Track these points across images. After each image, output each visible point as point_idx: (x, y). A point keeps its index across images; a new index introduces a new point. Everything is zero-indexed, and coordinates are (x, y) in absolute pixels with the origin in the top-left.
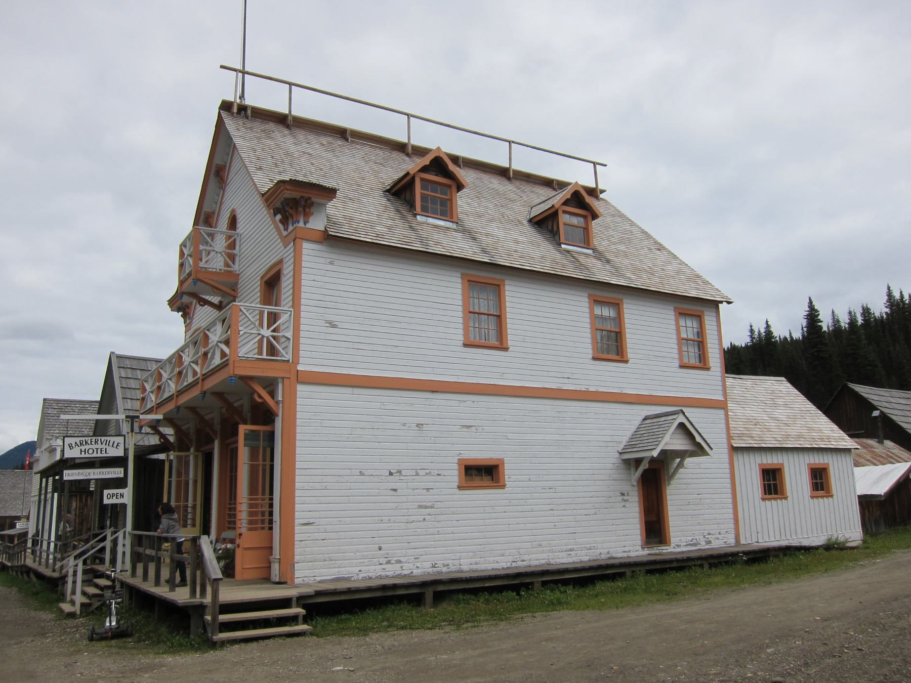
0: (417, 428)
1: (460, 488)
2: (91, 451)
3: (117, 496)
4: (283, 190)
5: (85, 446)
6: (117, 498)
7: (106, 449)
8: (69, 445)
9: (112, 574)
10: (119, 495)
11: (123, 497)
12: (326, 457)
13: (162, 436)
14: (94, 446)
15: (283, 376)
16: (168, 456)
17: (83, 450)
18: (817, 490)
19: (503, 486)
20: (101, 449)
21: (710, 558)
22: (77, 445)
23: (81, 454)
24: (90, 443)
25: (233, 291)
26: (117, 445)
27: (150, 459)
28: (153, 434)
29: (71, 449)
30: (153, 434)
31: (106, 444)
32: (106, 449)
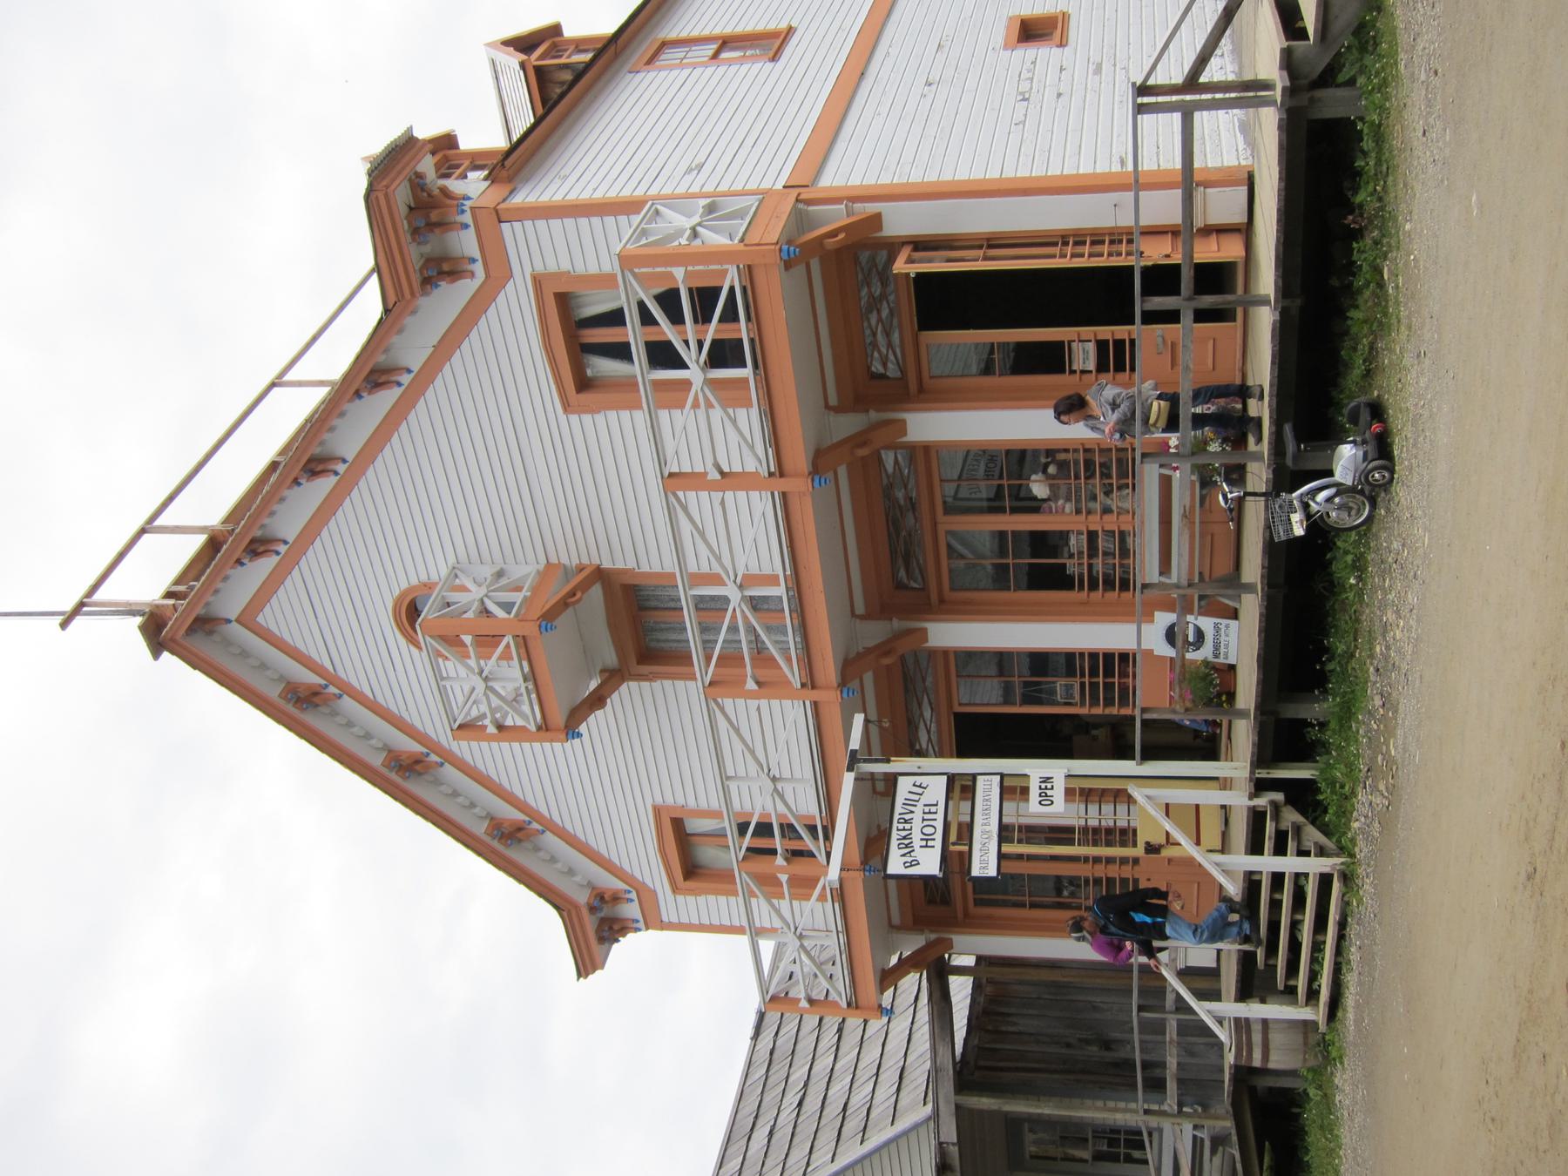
0: (934, 87)
1: (1064, 43)
2: (929, 830)
3: (1046, 788)
4: (386, 195)
5: (913, 840)
6: (1052, 788)
7: (925, 805)
8: (906, 867)
9: (1232, 499)
10: (1043, 786)
11: (1052, 778)
12: (979, 155)
13: (905, 966)
14: (917, 824)
15: (794, 199)
16: (961, 971)
17: (924, 843)
18: (1119, 344)
19: (1065, 16)
20: (924, 813)
21: (1271, 962)
22: (910, 852)
23: (933, 847)
24: (908, 832)
25: (582, 573)
26: (920, 786)
27: (963, 1054)
28: (895, 989)
29: (918, 864)
30: (895, 989)
31: (915, 806)
32: (925, 805)
